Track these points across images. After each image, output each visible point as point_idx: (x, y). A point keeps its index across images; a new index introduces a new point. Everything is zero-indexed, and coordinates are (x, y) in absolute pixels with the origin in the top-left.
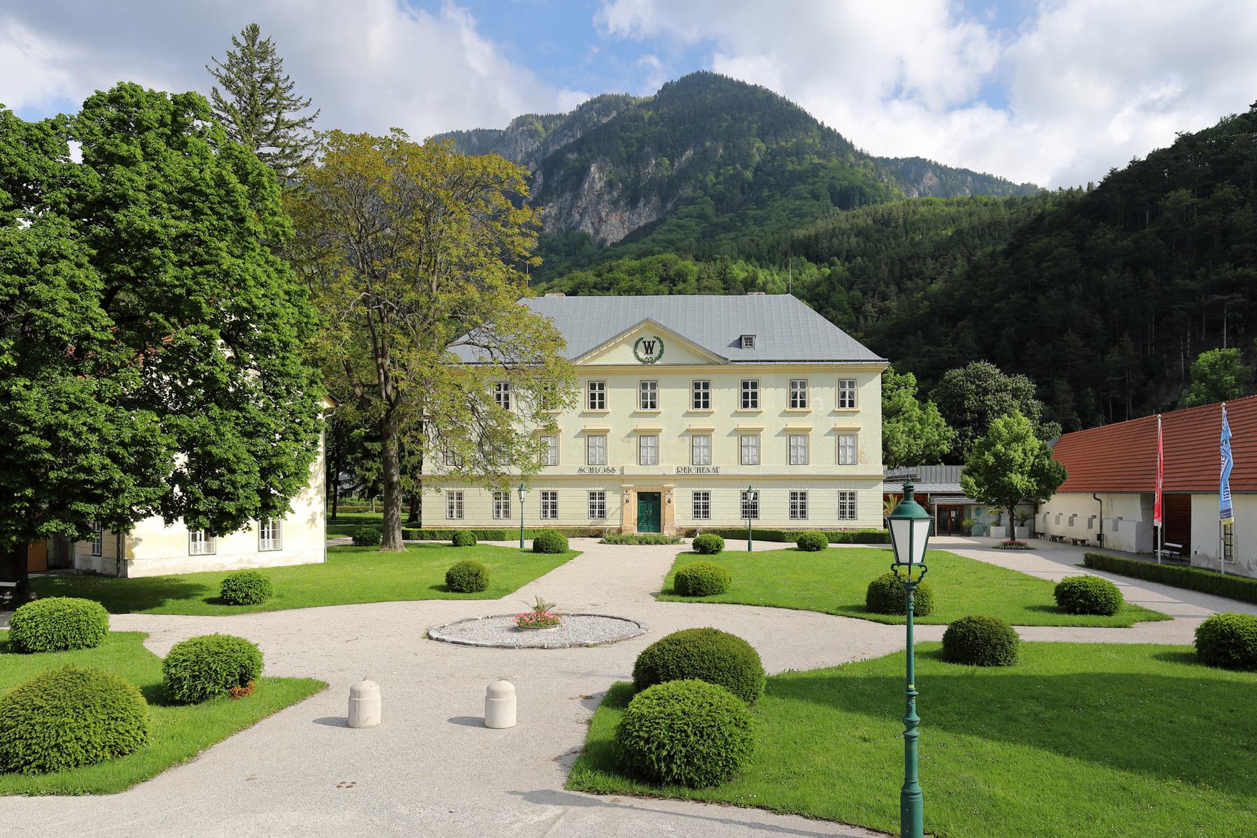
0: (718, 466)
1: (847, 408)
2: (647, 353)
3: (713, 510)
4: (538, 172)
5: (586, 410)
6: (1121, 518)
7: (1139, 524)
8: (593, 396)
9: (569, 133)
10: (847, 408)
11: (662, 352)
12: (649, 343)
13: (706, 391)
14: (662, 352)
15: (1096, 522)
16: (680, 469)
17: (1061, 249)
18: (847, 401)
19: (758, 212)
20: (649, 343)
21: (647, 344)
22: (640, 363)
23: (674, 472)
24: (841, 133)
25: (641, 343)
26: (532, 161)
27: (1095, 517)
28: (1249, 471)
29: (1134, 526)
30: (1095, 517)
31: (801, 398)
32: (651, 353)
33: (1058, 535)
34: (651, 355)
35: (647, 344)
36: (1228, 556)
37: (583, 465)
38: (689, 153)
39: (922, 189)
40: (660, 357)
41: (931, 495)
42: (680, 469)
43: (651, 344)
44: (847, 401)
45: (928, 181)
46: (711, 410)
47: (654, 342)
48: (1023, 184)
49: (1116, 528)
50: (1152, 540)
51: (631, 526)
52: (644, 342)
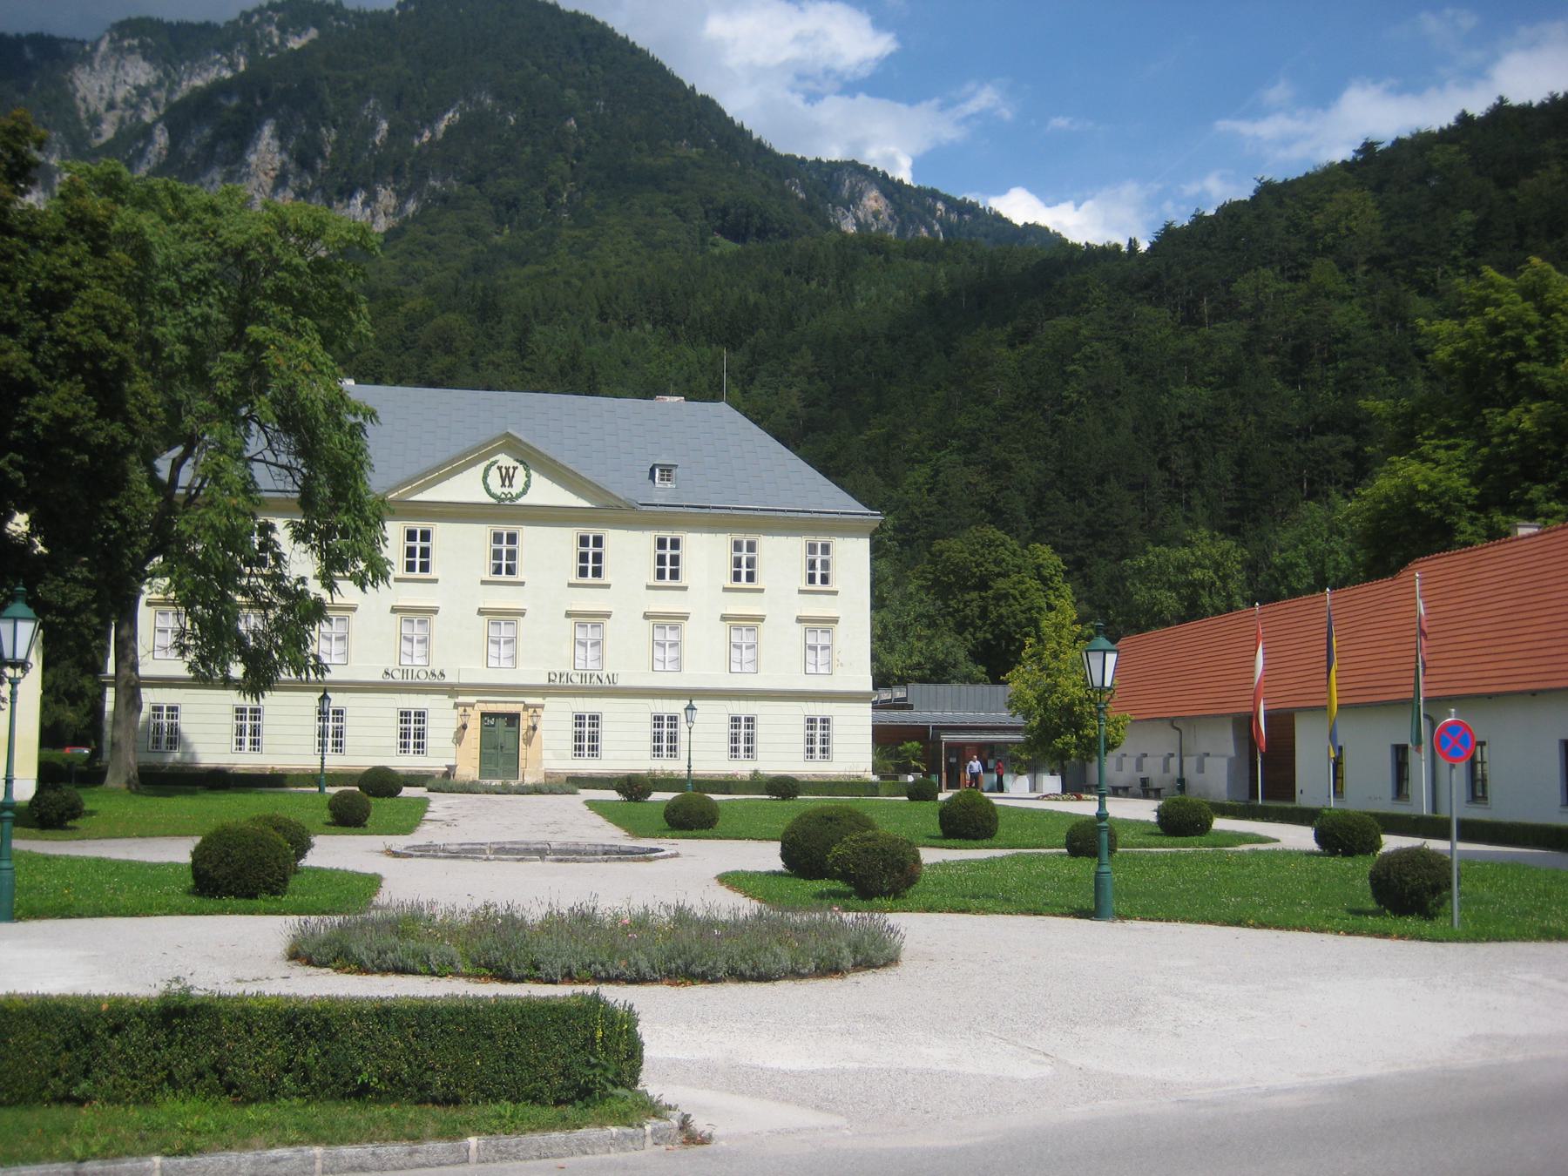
0: (616, 672)
1: (744, 583)
2: (503, 485)
3: (605, 743)
4: (160, 125)
5: (487, 577)
6: (1208, 755)
7: (1231, 760)
8: (738, 563)
9: (224, 60)
10: (744, 583)
11: (527, 485)
12: (507, 469)
13: (425, 544)
14: (527, 485)
15: (1174, 762)
16: (552, 677)
17: (1096, 345)
18: (818, 575)
19: (577, 233)
20: (507, 469)
21: (504, 471)
22: (492, 501)
23: (544, 681)
24: (664, 63)
25: (494, 468)
26: (146, 103)
27: (1172, 755)
28: (1359, 679)
29: (1224, 763)
30: (1172, 755)
31: (748, 566)
32: (511, 485)
33: (1122, 785)
34: (510, 490)
35: (504, 471)
36: (1338, 792)
37: (391, 666)
38: (450, 116)
39: (860, 214)
40: (524, 492)
41: (934, 727)
42: (552, 677)
43: (511, 471)
44: (818, 575)
45: (872, 203)
46: (606, 582)
47: (515, 468)
48: (1026, 224)
49: (1201, 769)
50: (1247, 782)
51: (469, 769)
52: (500, 468)
